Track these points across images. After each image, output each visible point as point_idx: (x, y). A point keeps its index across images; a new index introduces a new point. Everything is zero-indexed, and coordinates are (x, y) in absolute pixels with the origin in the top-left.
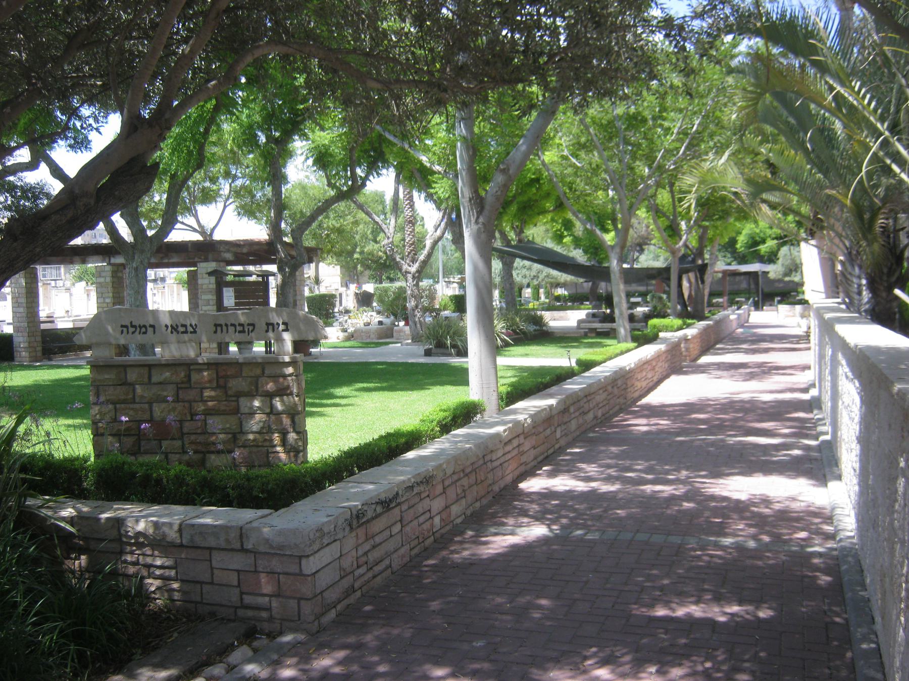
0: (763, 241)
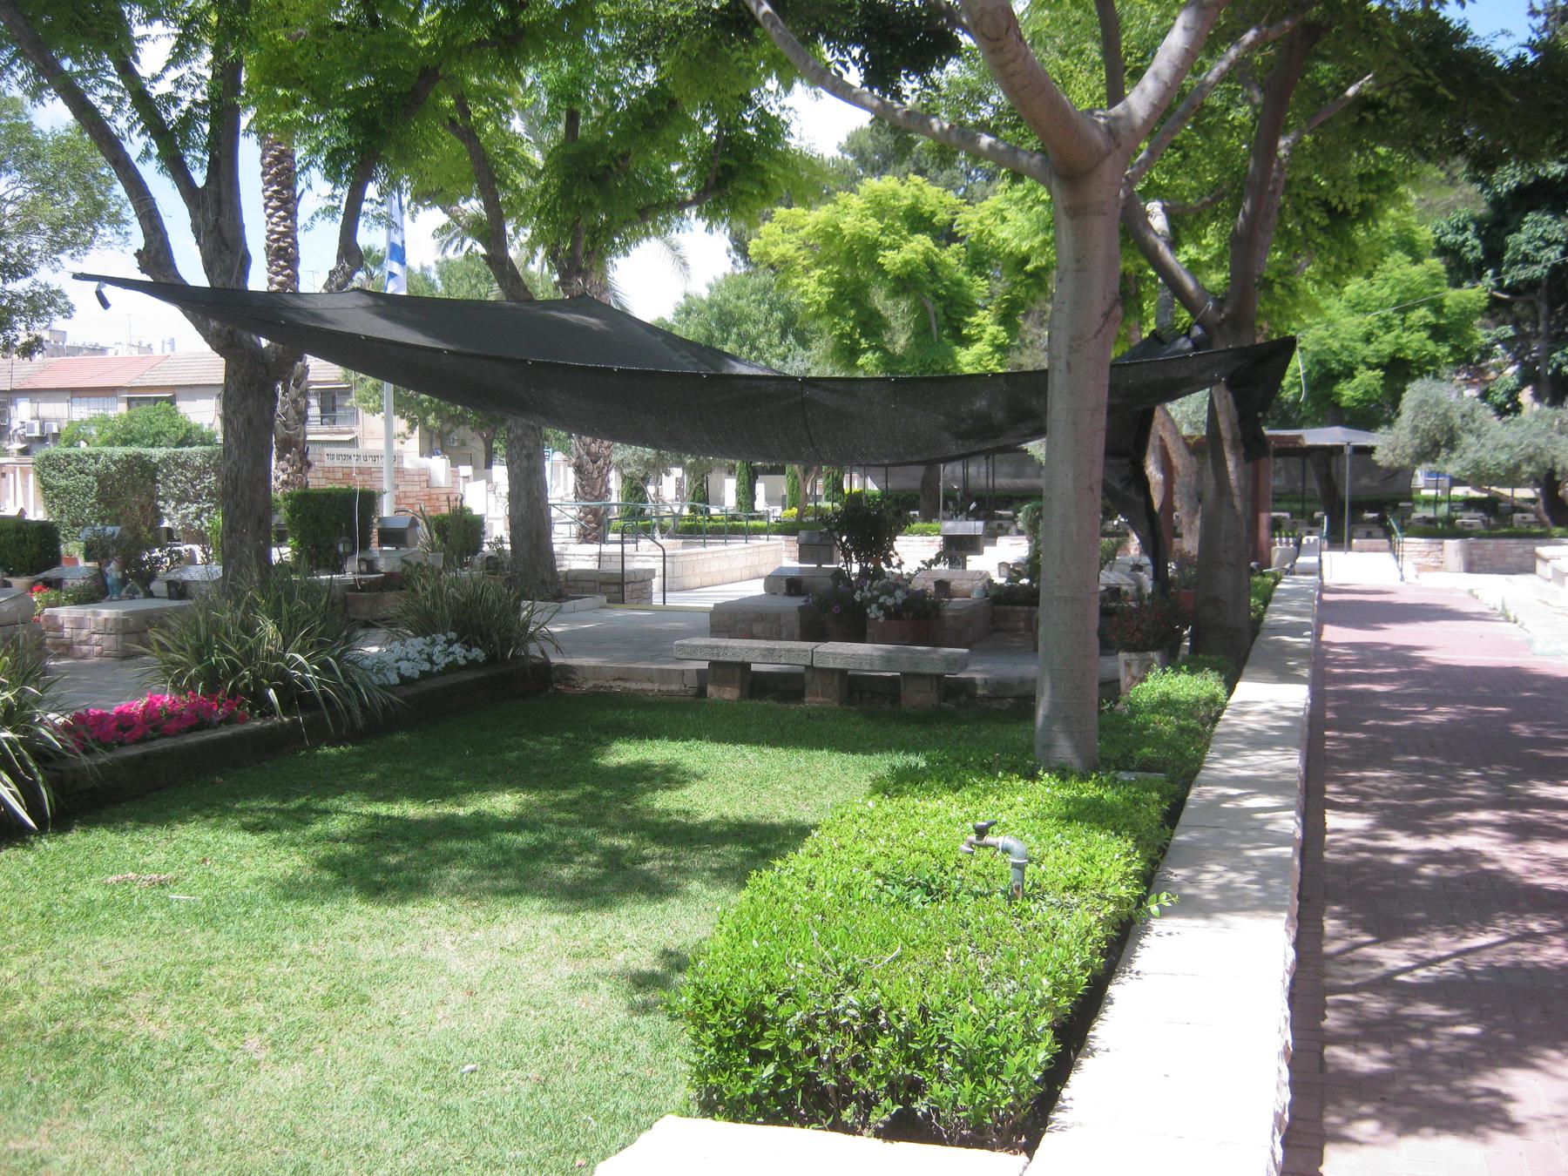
0: (1349, 373)
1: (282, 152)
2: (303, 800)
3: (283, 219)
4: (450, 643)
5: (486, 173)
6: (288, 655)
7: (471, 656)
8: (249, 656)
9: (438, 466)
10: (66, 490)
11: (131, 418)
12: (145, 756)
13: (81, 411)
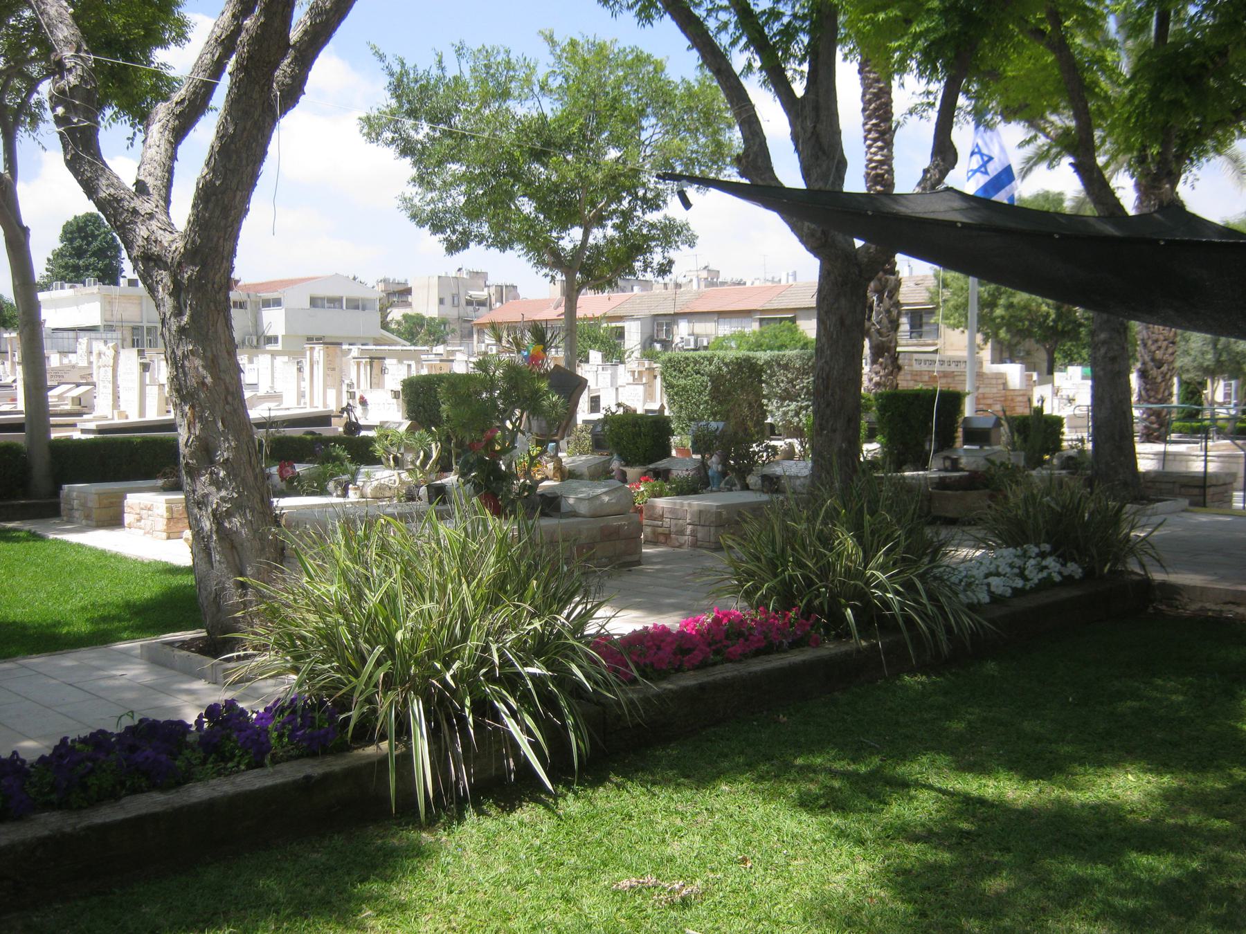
1: (880, 89)
2: (876, 761)
3: (881, 149)
4: (1043, 555)
5: (1075, 85)
6: (869, 573)
7: (1066, 572)
8: (825, 571)
9: (1013, 373)
10: (684, 388)
11: (762, 334)
12: (702, 688)
13: (725, 329)
